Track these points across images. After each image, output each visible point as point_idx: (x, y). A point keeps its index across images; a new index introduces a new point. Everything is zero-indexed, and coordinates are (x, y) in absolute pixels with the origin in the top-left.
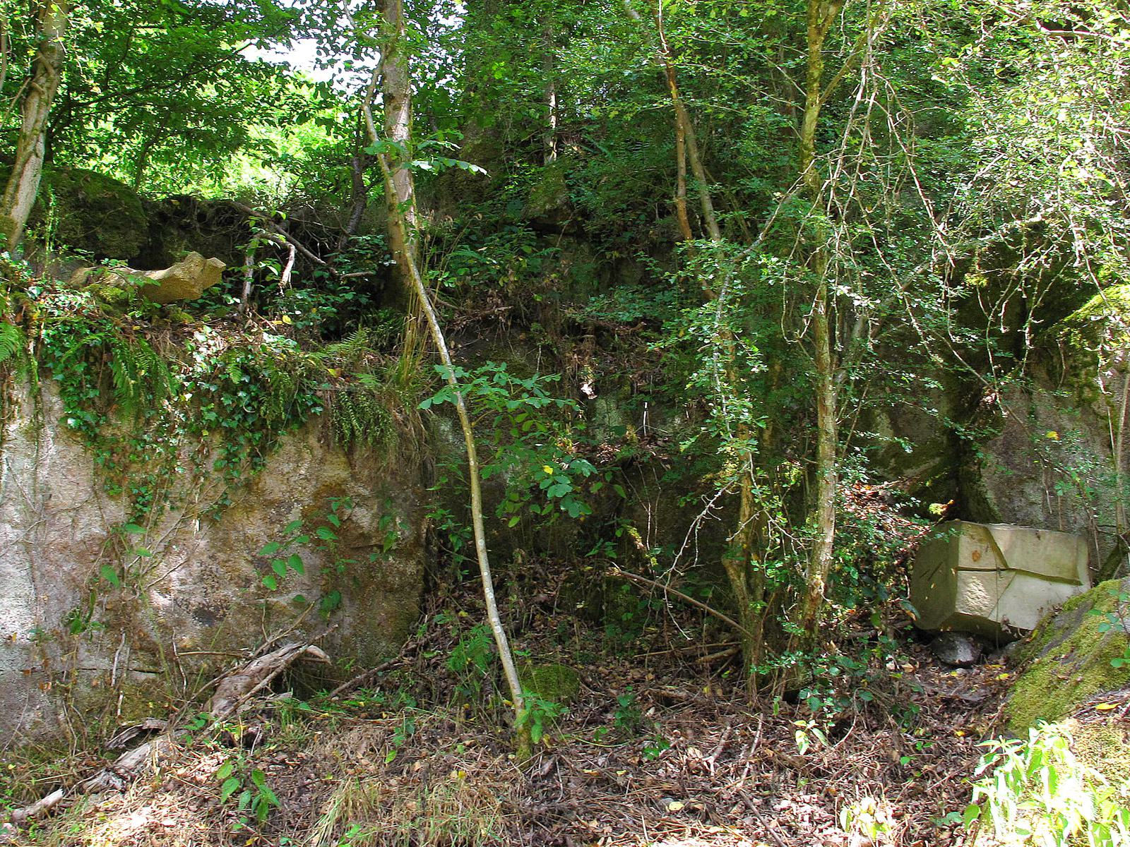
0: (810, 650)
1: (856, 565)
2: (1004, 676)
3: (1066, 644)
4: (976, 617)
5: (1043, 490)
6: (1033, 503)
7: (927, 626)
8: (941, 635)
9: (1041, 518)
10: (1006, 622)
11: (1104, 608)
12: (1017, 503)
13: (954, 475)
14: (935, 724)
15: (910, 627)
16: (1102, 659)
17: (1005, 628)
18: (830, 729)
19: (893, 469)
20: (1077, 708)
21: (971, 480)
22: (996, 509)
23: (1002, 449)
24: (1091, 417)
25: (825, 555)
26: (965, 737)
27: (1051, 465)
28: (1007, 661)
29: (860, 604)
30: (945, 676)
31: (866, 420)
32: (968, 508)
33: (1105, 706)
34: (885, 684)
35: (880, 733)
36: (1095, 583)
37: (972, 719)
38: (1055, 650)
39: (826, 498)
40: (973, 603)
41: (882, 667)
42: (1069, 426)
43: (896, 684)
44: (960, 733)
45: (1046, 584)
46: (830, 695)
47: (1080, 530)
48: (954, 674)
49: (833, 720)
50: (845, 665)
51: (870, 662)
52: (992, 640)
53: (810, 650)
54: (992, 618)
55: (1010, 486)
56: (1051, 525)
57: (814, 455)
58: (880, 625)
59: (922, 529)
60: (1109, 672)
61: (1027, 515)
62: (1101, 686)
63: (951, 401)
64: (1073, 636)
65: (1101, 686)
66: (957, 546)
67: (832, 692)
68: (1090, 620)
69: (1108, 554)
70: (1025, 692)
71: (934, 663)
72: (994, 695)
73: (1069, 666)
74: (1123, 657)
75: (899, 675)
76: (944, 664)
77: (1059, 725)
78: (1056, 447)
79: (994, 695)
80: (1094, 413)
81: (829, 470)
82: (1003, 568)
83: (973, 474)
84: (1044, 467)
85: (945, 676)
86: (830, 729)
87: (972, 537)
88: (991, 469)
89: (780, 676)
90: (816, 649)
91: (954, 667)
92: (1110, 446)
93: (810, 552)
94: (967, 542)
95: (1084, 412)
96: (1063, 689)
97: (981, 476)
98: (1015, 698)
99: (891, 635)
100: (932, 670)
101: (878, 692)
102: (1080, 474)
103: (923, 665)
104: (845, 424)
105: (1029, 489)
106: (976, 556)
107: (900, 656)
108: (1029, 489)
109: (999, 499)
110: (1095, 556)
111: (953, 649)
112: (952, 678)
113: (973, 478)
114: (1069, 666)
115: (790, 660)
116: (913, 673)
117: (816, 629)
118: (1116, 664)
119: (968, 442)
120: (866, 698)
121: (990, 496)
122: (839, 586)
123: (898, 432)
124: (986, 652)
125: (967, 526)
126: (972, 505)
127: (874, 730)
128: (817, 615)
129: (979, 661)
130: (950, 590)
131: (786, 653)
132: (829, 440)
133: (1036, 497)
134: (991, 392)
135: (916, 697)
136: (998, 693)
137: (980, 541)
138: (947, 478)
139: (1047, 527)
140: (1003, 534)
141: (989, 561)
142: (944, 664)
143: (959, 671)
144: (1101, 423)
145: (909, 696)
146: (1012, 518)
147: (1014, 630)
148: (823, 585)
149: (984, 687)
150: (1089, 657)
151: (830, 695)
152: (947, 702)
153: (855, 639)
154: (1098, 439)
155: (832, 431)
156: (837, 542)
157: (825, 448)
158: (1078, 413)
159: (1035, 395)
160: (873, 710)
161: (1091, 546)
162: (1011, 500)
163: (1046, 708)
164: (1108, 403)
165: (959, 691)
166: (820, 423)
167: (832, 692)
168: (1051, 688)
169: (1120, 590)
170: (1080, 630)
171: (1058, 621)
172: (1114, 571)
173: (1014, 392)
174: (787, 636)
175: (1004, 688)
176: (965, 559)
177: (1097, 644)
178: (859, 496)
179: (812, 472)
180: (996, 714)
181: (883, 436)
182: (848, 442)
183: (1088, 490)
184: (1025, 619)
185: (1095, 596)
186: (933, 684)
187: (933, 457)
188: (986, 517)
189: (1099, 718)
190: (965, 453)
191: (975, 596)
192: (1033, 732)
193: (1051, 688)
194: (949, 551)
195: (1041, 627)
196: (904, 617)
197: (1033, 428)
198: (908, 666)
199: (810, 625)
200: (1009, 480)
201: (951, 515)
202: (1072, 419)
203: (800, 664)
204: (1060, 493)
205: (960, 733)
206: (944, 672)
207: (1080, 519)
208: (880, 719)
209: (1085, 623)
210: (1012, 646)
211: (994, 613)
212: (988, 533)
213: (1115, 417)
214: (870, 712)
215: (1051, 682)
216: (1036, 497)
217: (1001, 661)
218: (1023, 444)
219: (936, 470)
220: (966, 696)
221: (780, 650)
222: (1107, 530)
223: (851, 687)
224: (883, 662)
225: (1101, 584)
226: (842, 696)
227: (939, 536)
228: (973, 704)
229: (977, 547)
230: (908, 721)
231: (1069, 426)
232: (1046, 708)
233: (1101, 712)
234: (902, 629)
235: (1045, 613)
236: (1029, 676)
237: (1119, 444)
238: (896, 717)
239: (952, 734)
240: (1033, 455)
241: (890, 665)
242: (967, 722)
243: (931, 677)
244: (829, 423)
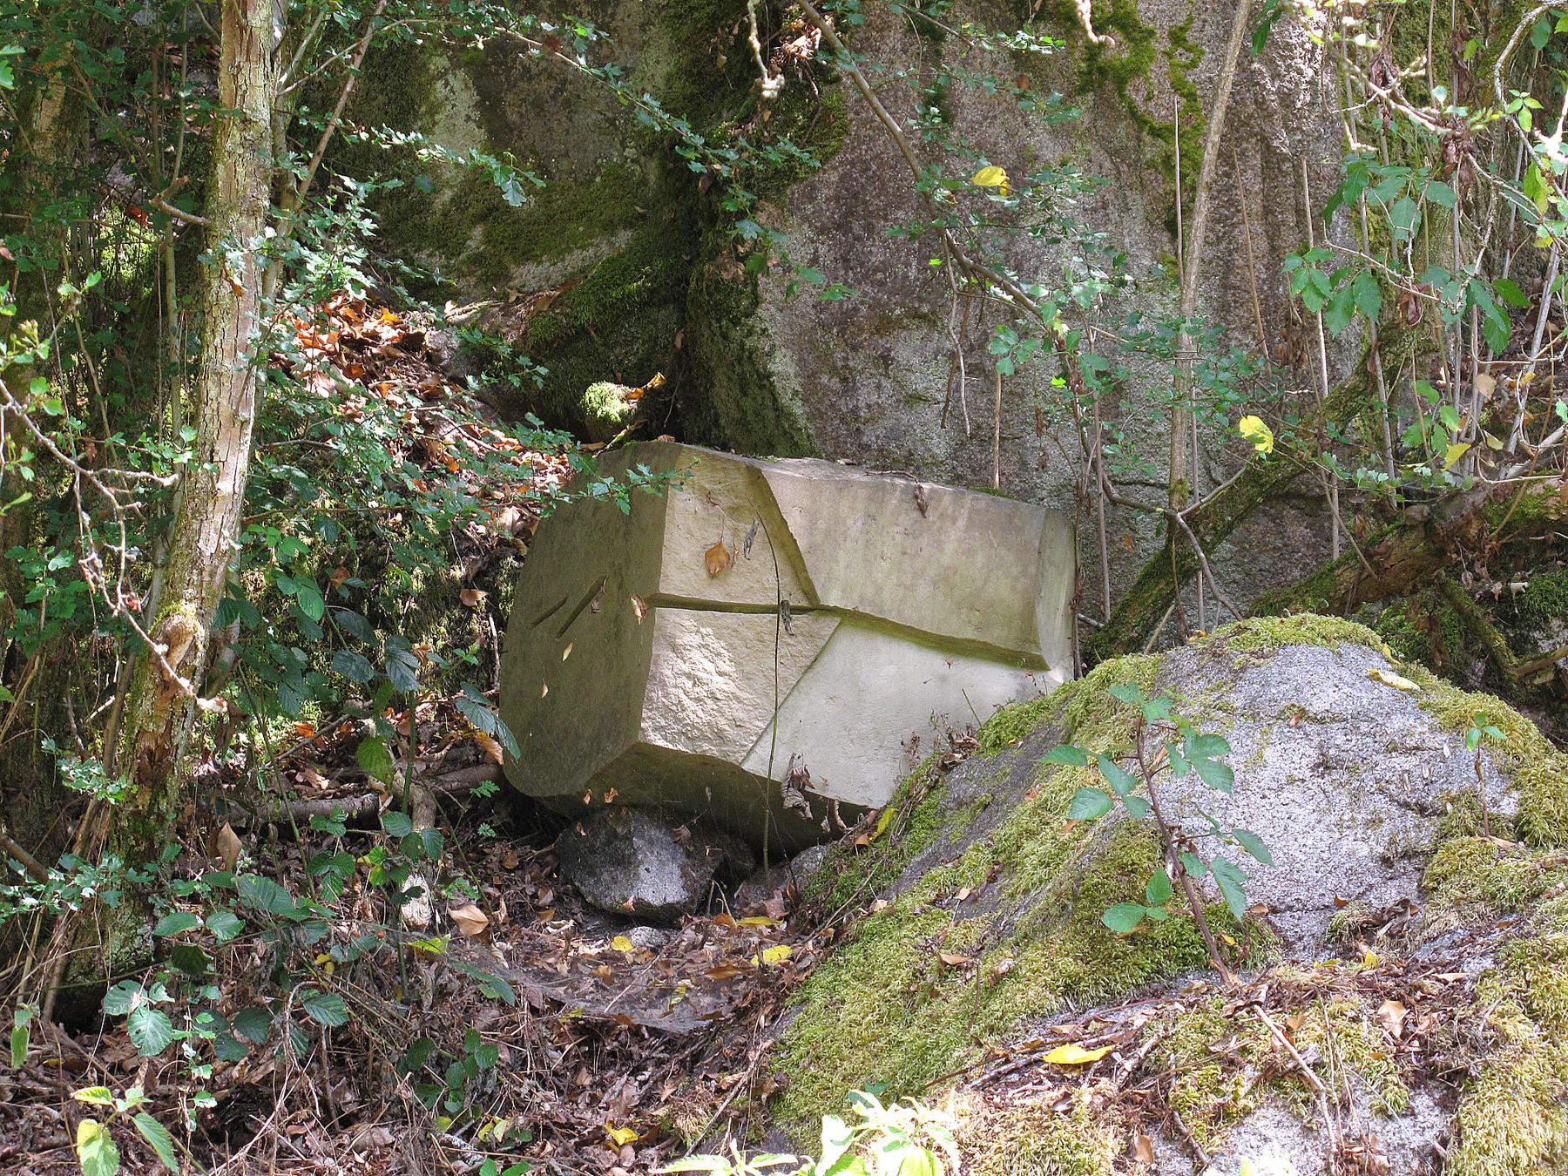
0: (152, 854)
1: (322, 580)
2: (775, 955)
3: (977, 858)
4: (706, 761)
5: (953, 356)
6: (916, 398)
7: (541, 785)
8: (585, 814)
9: (940, 446)
10: (798, 781)
11: (1102, 745)
12: (866, 395)
13: (673, 293)
14: (548, 1103)
15: (488, 788)
16: (1079, 905)
17: (793, 799)
18: (201, 1115)
19: (477, 259)
20: (990, 1058)
21: (721, 311)
22: (798, 409)
23: (831, 213)
24: (1122, 128)
25: (216, 535)
26: (638, 1147)
27: (979, 273)
28: (794, 904)
29: (333, 710)
30: (592, 950)
31: (396, 84)
32: (708, 404)
33: (1072, 1054)
34: (389, 971)
35: (364, 1132)
36: (1087, 660)
37: (667, 1091)
38: (940, 872)
39: (232, 343)
40: (696, 714)
41: (389, 913)
42: (1051, 152)
43: (428, 974)
44: (622, 1135)
45: (934, 662)
46: (204, 1005)
47: (1058, 492)
48: (624, 944)
49: (211, 1086)
50: (262, 903)
51: (349, 899)
52: (753, 835)
53: (152, 854)
54: (754, 766)
55: (851, 335)
56: (967, 474)
57: (199, 196)
58: (390, 774)
59: (547, 469)
60: (1097, 944)
61: (895, 435)
62: (1069, 990)
63: (682, 44)
64: (1004, 831)
65: (1069, 990)
66: (660, 527)
67: (213, 993)
68: (1056, 781)
69: (1139, 572)
70: (845, 1004)
71: (561, 908)
72: (741, 1013)
73: (977, 928)
74: (1142, 901)
75: (438, 945)
76: (593, 910)
77: (923, 1112)
78: (1007, 220)
79: (741, 1013)
80: (1133, 113)
81: (242, 250)
82: (802, 605)
83: (729, 290)
84: (945, 273)
85: (592, 950)
86: (201, 1115)
87: (709, 498)
88: (790, 268)
89: (45, 936)
90: (169, 852)
91: (622, 921)
92: (1171, 226)
93: (161, 521)
94: (692, 516)
95: (1104, 107)
96: (952, 1002)
97: (756, 301)
98: (804, 1026)
99: (424, 813)
100: (554, 930)
101: (367, 998)
102: (1071, 312)
103: (523, 913)
104: (315, 94)
105: (907, 349)
106: (717, 562)
107: (446, 879)
108: (907, 349)
109: (810, 377)
110: (1097, 581)
111: (625, 863)
112: (613, 958)
113: (732, 306)
114: (977, 928)
115: (82, 883)
116: (485, 938)
117: (173, 784)
118: (1119, 921)
119: (718, 186)
120: (327, 1016)
121: (783, 366)
122: (253, 651)
123: (499, 135)
124: (729, 877)
125: (694, 456)
126: (723, 394)
127: (347, 1122)
128: (179, 737)
129: (703, 905)
130: (626, 671)
131: (67, 861)
132: (253, 146)
133: (928, 378)
134: (811, 24)
135: (490, 1015)
136: (755, 1006)
137: (734, 511)
138: (650, 300)
139: (956, 479)
140: (789, 478)
141: (758, 578)
142: (593, 910)
143: (642, 934)
144: (1152, 150)
145: (468, 1012)
146: (846, 442)
147: (821, 805)
148: (202, 633)
149: (714, 990)
150: (1043, 899)
151: (204, 1005)
152: (591, 1033)
153: (302, 820)
154: (1138, 202)
155: (265, 114)
156: (262, 496)
157: (239, 172)
158: (1078, 114)
159: (949, 44)
160: (346, 1053)
161: (1084, 544)
162: (848, 382)
163: (898, 1057)
164: (1177, 87)
165: (632, 1000)
166: (224, 88)
167: (213, 993)
168: (919, 993)
169: (1155, 690)
170: (1022, 813)
171: (955, 773)
172: (1148, 629)
173: (884, 28)
174: (76, 805)
175: (775, 991)
176: (680, 569)
177: (1070, 858)
178: (357, 345)
179: (189, 255)
180: (742, 1076)
181: (447, 146)
182: (319, 150)
183: (1089, 362)
184: (861, 776)
185: (1076, 705)
186: (547, 976)
187: (610, 227)
188: (762, 432)
189: (1049, 1094)
190: (713, 220)
191: (703, 688)
192: (834, 1130)
193: (919, 993)
194: (634, 533)
195: (906, 800)
196: (470, 752)
197: (933, 154)
198: (470, 914)
199: (153, 770)
200: (845, 320)
201: (653, 421)
202: (1062, 131)
203: (111, 897)
204: (1005, 367)
205: (622, 1135)
206: (591, 937)
207: (1060, 455)
208: (368, 1082)
209: (1042, 791)
210: (813, 860)
211: (763, 751)
212: (757, 480)
213: (1193, 131)
214: (340, 1062)
215: (919, 974)
216: (928, 378)
217: (775, 905)
218: (899, 201)
219: (618, 270)
220: (654, 1017)
221: (50, 849)
222: (1141, 495)
223: (278, 977)
224: (391, 897)
225: (1099, 670)
226: (244, 1009)
227: (599, 488)
228: (672, 1043)
229: (725, 533)
230: (458, 1091)
231: (1051, 152)
232: (898, 1057)
233: (1061, 1074)
234: (463, 794)
235: (925, 754)
236: (853, 954)
237: (1200, 220)
238: (422, 1082)
239: (599, 1137)
240: (931, 240)
241: (416, 911)
242: (648, 1099)
243: (544, 950)
244: (259, 90)
